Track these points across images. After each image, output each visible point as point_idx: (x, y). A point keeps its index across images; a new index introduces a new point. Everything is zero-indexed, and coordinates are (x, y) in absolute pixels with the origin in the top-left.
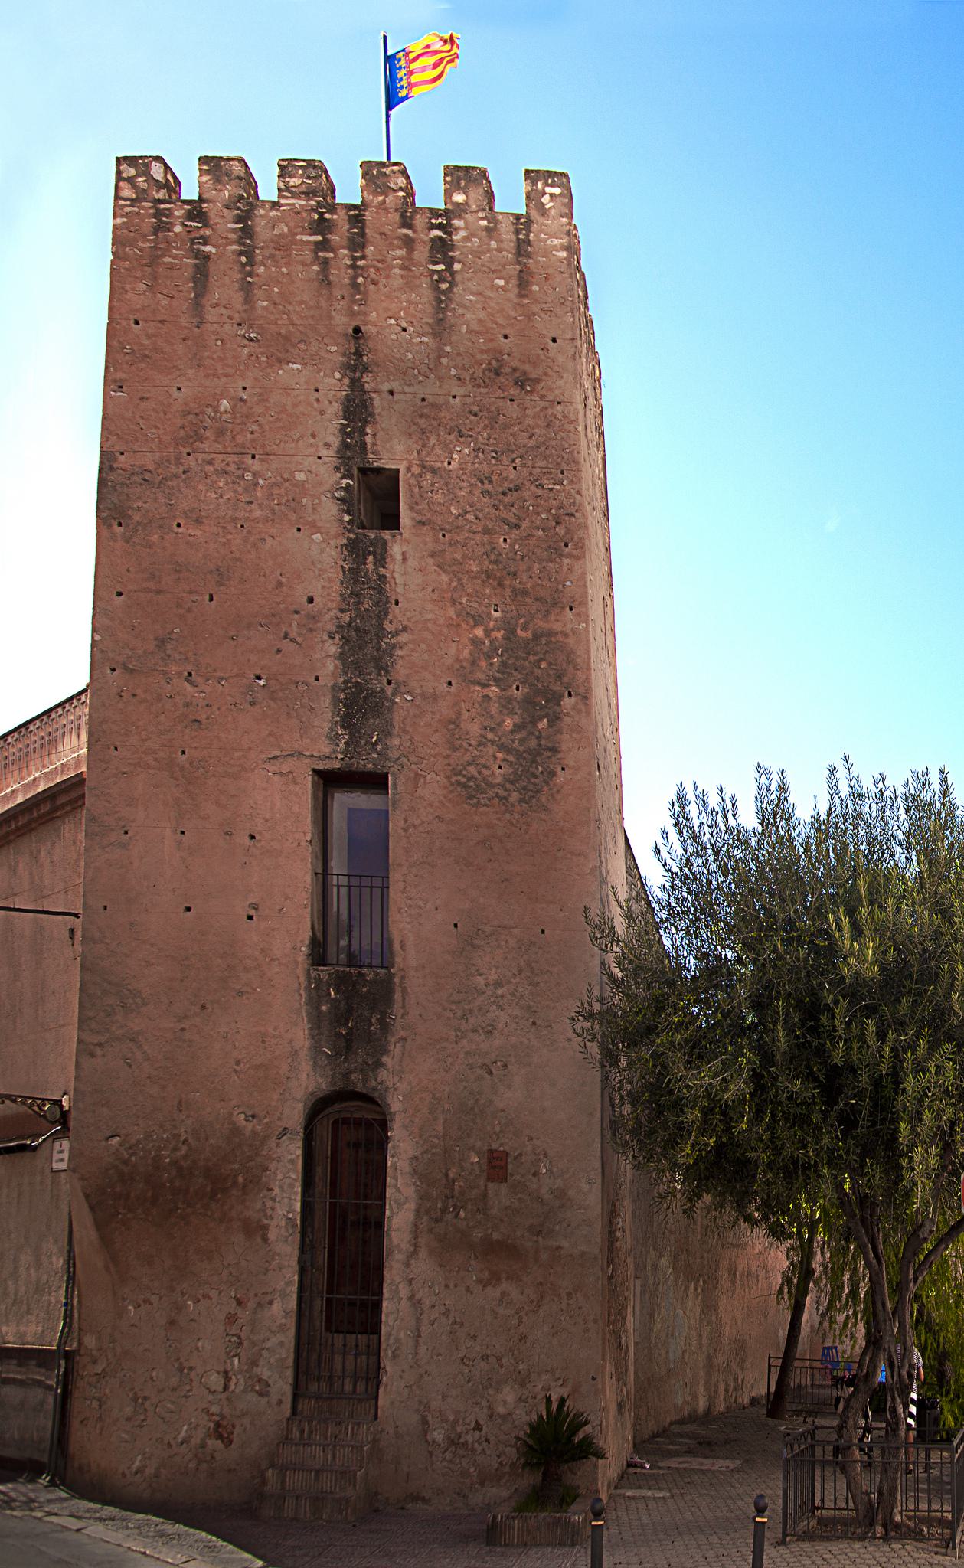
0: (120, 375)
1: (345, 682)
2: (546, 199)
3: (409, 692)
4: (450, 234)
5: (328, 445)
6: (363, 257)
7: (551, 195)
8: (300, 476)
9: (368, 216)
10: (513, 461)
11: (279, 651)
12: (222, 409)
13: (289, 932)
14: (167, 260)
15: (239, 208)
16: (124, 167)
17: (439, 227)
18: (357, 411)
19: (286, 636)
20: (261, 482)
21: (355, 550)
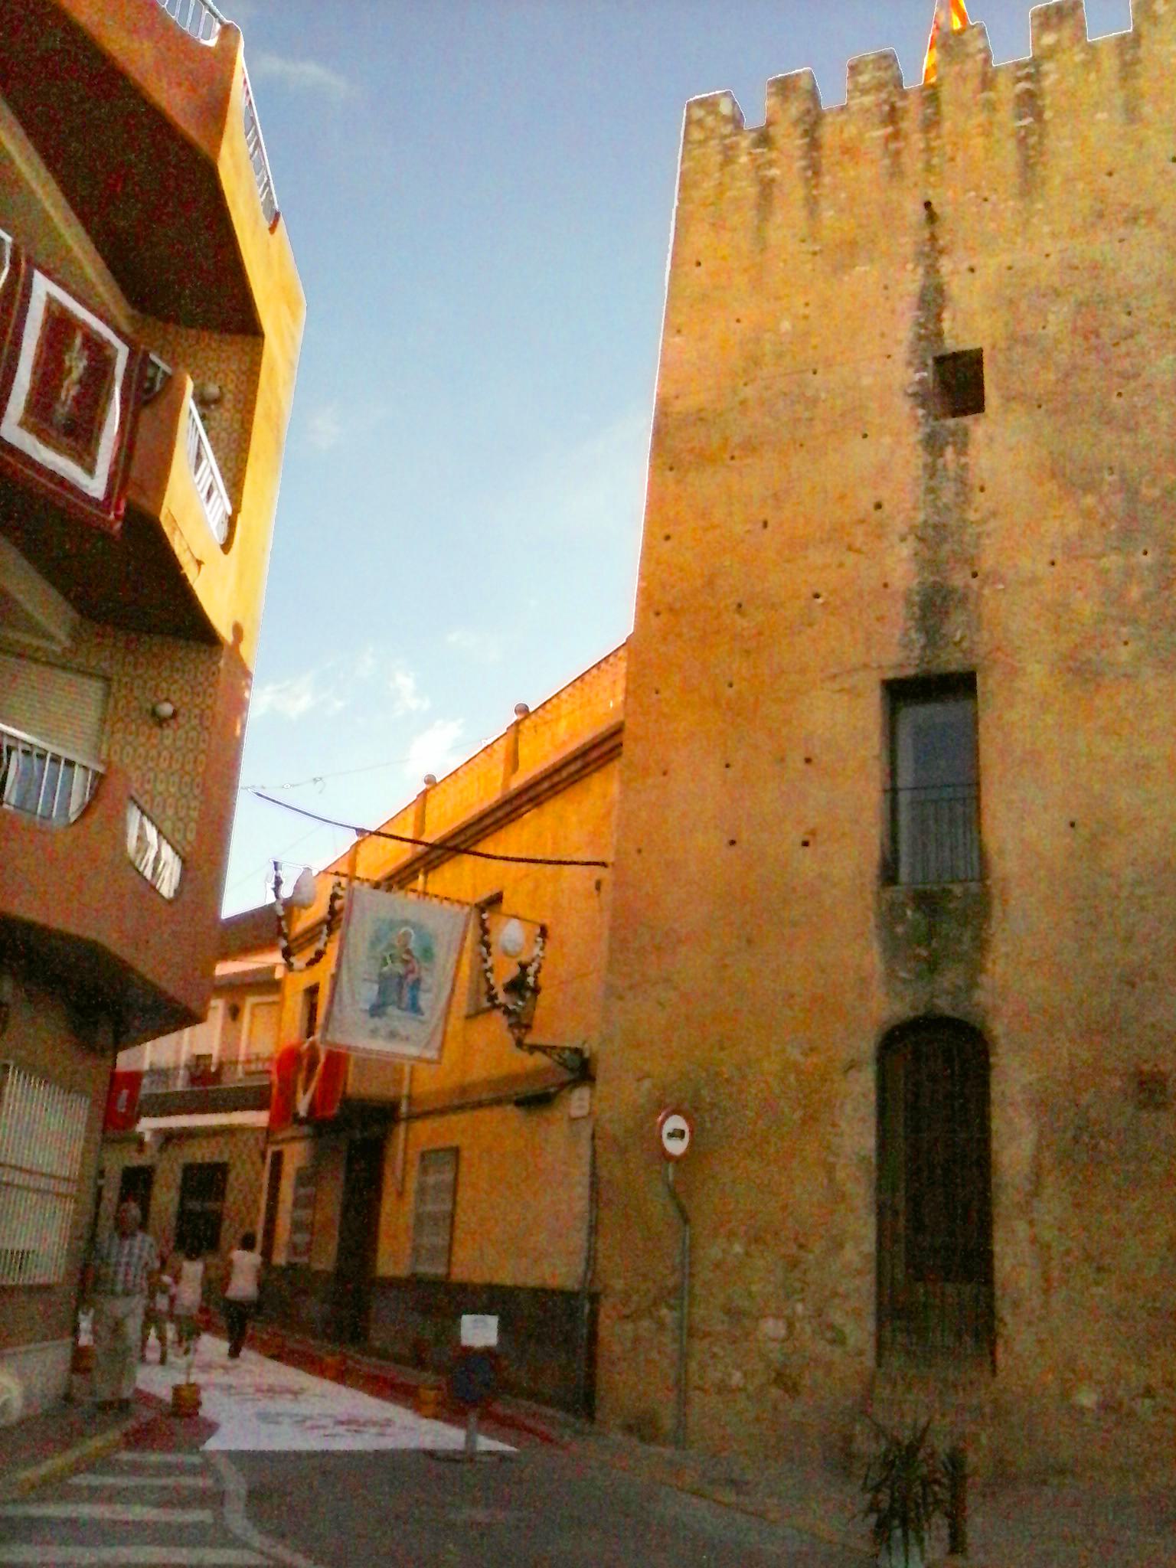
0: (680, 319)
5: (898, 342)
6: (939, 137)
9: (945, 93)
13: (852, 857)
21: (933, 444)
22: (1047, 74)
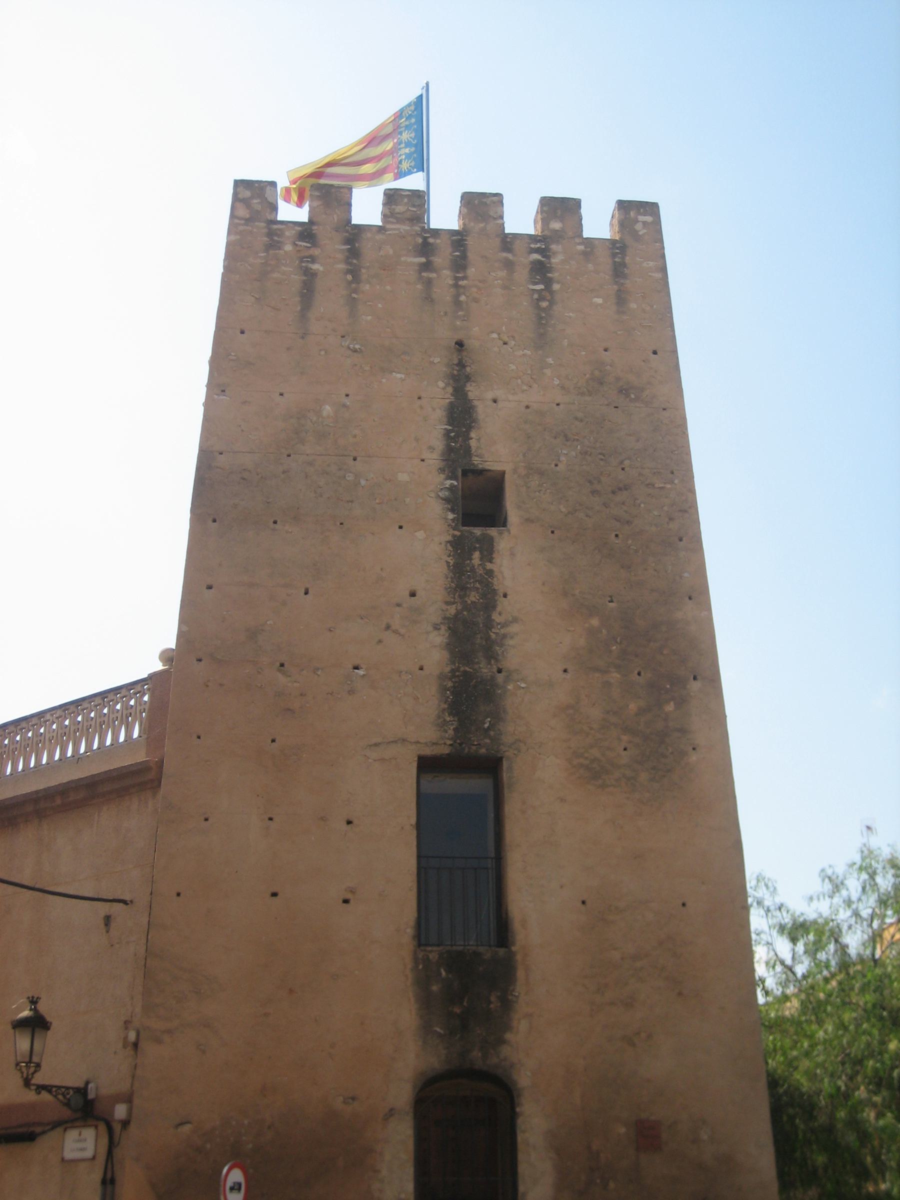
1: (453, 671)
2: (639, 227)
3: (523, 680)
4: (548, 257)
5: (431, 449)
7: (644, 223)
8: (403, 477)
9: (470, 241)
10: (622, 462)
11: (380, 641)
12: (325, 414)
14: (275, 275)
15: (347, 231)
16: (240, 189)
17: (537, 251)
18: (461, 417)
19: (388, 627)
20: (363, 482)
21: (460, 548)
22: (555, 253)
